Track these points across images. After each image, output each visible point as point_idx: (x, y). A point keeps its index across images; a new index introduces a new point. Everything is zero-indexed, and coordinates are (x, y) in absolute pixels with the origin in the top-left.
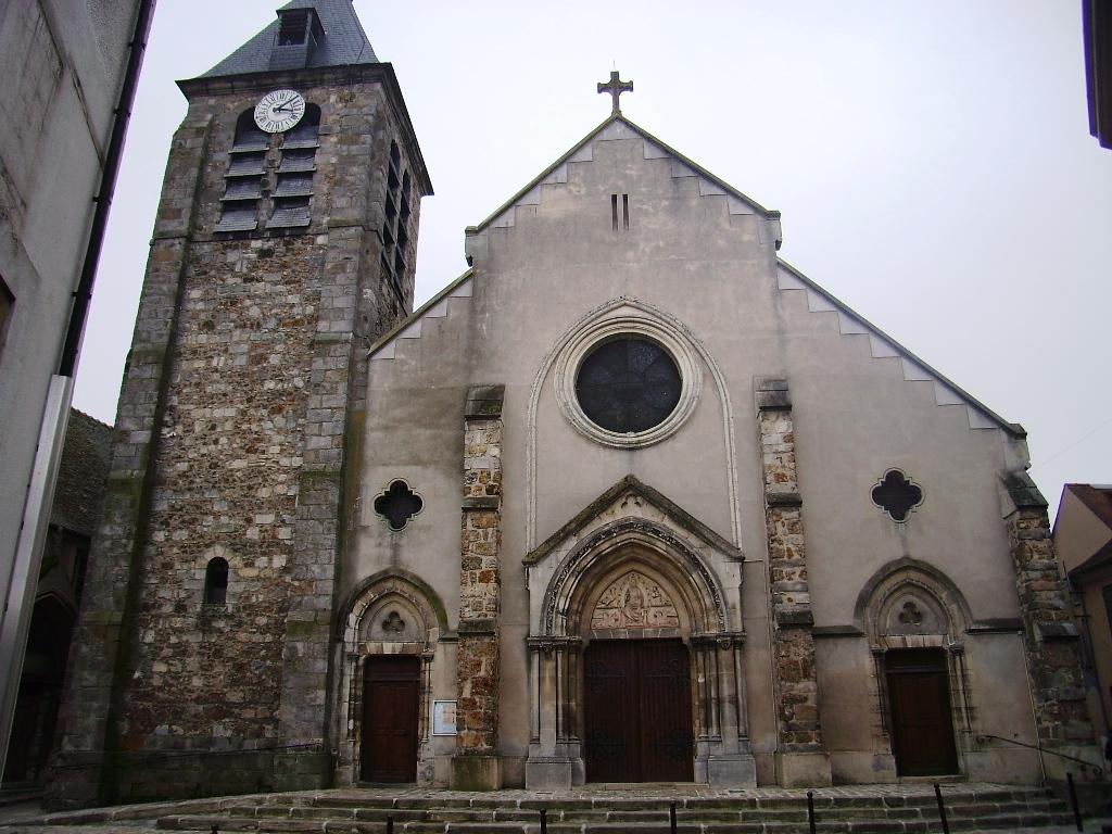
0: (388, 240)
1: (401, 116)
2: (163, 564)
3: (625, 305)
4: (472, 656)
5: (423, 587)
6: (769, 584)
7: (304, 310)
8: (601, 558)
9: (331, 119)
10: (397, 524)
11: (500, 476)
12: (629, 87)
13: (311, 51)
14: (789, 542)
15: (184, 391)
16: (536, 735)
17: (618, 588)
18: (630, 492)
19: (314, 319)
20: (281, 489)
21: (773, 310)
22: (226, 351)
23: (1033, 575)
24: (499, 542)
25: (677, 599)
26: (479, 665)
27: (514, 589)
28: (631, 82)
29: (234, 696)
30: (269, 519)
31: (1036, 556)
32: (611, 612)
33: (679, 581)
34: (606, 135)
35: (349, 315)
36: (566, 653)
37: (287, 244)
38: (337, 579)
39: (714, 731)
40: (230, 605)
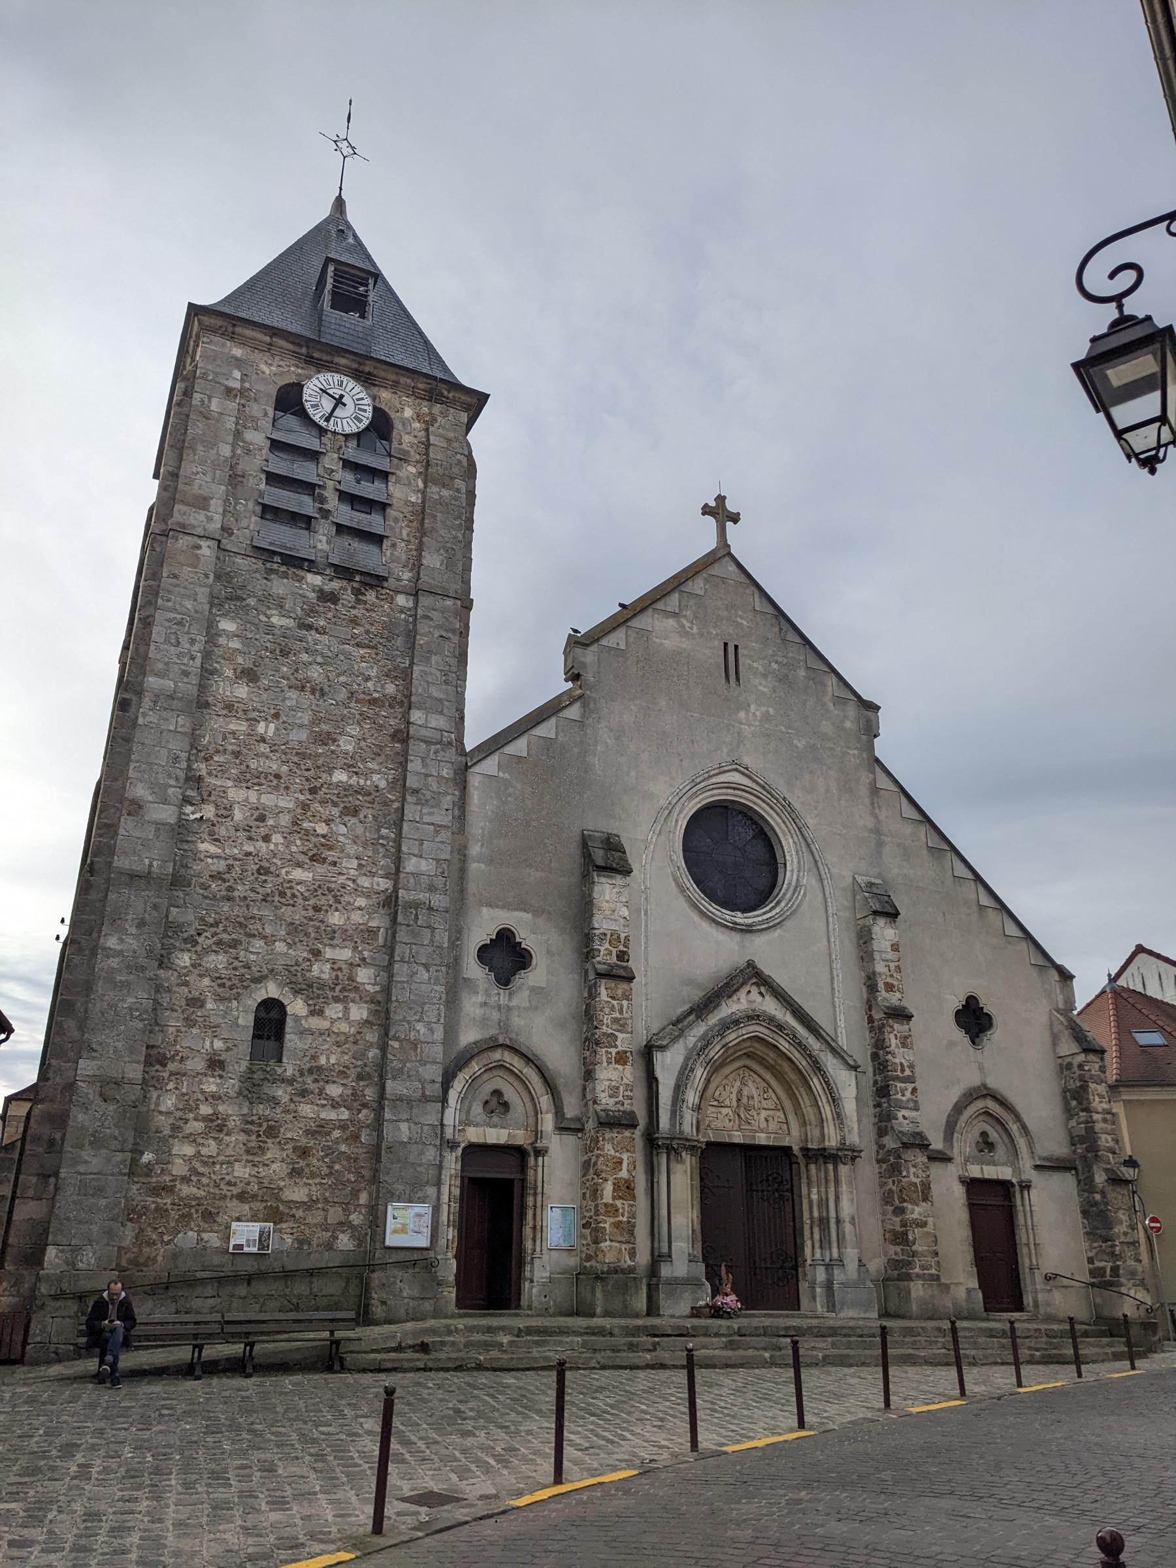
2: (187, 999)
3: (736, 770)
4: (612, 1152)
7: (383, 687)
9: (407, 439)
10: (504, 980)
15: (216, 758)
18: (754, 980)
20: (357, 917)
30: (345, 954)
37: (357, 593)
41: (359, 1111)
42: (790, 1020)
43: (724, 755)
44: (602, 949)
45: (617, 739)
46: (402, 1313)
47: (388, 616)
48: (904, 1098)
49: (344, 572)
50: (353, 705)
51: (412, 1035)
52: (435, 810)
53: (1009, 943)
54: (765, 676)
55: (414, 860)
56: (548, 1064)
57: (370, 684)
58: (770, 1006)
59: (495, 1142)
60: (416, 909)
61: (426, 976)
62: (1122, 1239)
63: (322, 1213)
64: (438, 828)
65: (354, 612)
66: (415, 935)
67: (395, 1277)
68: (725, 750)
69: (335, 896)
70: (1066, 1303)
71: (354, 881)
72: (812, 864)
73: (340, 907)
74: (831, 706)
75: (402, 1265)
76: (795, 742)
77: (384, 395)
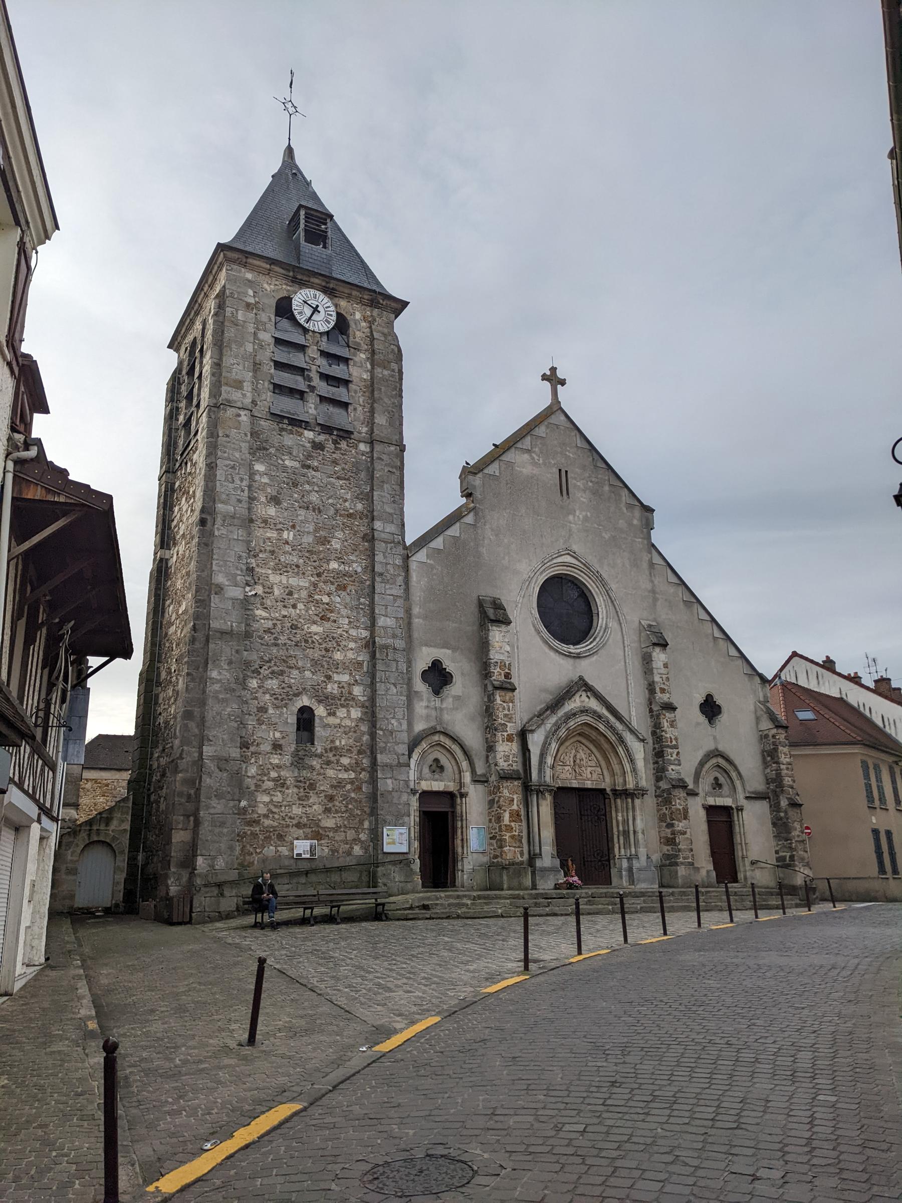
3: (568, 554)
20: (350, 655)
22: (293, 527)
29: (329, 822)
37: (335, 442)
40: (319, 748)
41: (360, 773)
42: (605, 712)
45: (497, 535)
49: (327, 429)
51: (390, 727)
54: (584, 491)
55: (383, 618)
57: (347, 504)
58: (594, 704)
61: (395, 691)
62: (797, 839)
65: (334, 456)
69: (337, 642)
75: (394, 863)
76: (604, 534)
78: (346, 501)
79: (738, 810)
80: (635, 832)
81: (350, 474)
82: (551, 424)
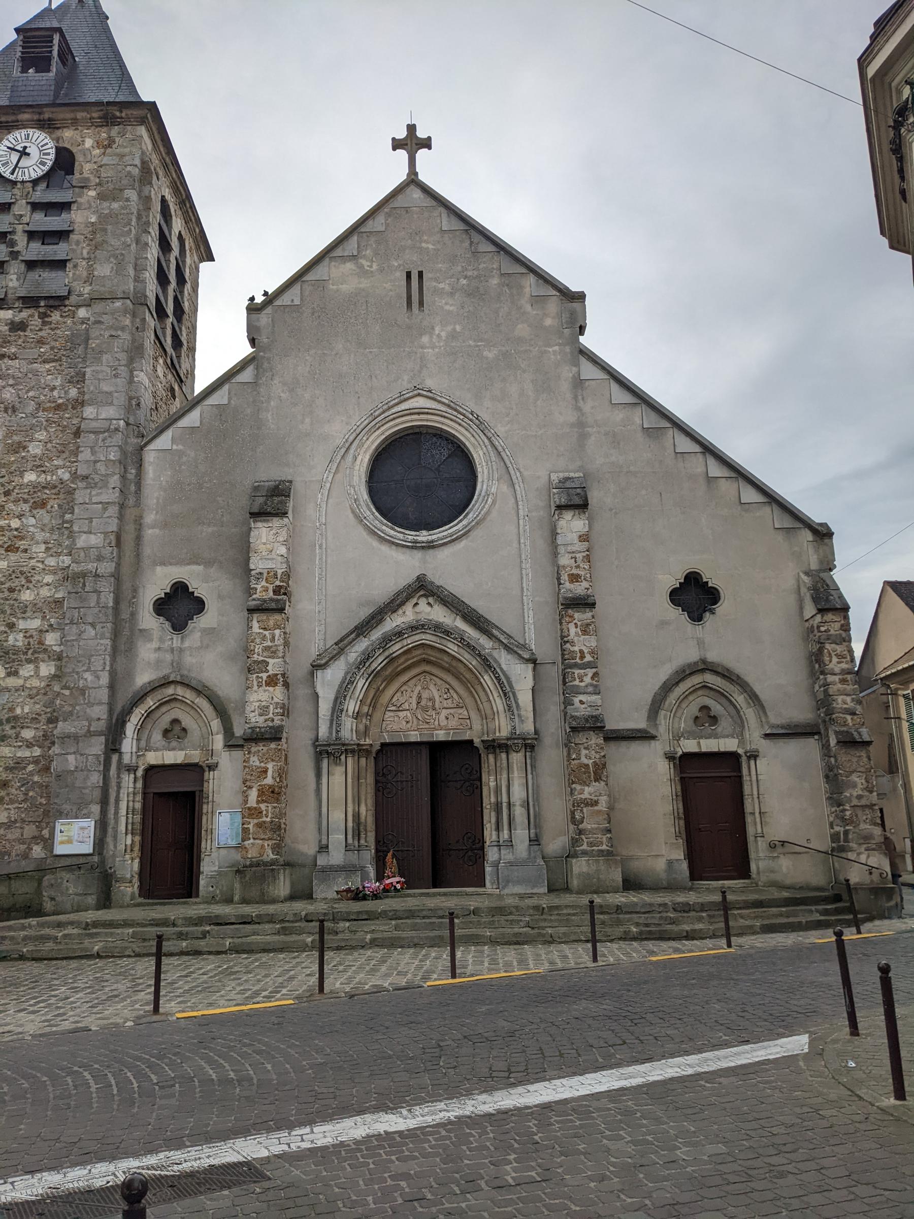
0: (161, 312)
1: (171, 167)
3: (419, 395)
4: (257, 763)
5: (202, 691)
6: (561, 686)
7: (66, 393)
8: (392, 660)
9: (87, 167)
10: (179, 627)
11: (287, 575)
12: (426, 144)
13: (59, 84)
14: (581, 643)
16: (324, 842)
17: (409, 690)
18: (422, 593)
19: (79, 403)
20: (45, 592)
21: (574, 402)
23: (830, 678)
24: (286, 644)
25: (469, 701)
26: (265, 771)
27: (302, 692)
28: (429, 138)
31: (835, 660)
32: (401, 714)
33: (470, 683)
34: (400, 201)
35: (120, 399)
36: (356, 758)
37: (43, 316)
38: (112, 687)
39: (505, 834)
41: (50, 748)
42: (460, 624)
43: (405, 383)
44: (259, 587)
45: (292, 390)
46: (68, 906)
47: (70, 329)
48: (582, 684)
49: (30, 301)
50: (40, 414)
51: (81, 684)
52: (103, 490)
53: (746, 511)
54: (452, 294)
55: (84, 536)
56: (220, 693)
57: (55, 393)
58: (439, 614)
59: (172, 762)
60: (84, 578)
61: (93, 633)
62: (855, 802)
63: (19, 830)
64: (106, 505)
65: (40, 334)
66: (82, 599)
67: (61, 878)
68: (406, 378)
69: (27, 578)
70: (795, 870)
71: (43, 562)
72: (504, 471)
73: (31, 586)
74: (528, 308)
75: (68, 868)
76: (486, 353)
77: (66, 134)
78: (53, 389)
79: (749, 758)
80: (509, 804)
81: (62, 352)
82: (413, 206)
